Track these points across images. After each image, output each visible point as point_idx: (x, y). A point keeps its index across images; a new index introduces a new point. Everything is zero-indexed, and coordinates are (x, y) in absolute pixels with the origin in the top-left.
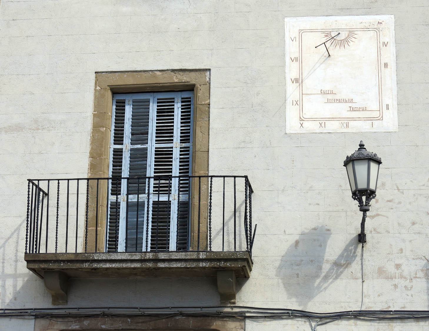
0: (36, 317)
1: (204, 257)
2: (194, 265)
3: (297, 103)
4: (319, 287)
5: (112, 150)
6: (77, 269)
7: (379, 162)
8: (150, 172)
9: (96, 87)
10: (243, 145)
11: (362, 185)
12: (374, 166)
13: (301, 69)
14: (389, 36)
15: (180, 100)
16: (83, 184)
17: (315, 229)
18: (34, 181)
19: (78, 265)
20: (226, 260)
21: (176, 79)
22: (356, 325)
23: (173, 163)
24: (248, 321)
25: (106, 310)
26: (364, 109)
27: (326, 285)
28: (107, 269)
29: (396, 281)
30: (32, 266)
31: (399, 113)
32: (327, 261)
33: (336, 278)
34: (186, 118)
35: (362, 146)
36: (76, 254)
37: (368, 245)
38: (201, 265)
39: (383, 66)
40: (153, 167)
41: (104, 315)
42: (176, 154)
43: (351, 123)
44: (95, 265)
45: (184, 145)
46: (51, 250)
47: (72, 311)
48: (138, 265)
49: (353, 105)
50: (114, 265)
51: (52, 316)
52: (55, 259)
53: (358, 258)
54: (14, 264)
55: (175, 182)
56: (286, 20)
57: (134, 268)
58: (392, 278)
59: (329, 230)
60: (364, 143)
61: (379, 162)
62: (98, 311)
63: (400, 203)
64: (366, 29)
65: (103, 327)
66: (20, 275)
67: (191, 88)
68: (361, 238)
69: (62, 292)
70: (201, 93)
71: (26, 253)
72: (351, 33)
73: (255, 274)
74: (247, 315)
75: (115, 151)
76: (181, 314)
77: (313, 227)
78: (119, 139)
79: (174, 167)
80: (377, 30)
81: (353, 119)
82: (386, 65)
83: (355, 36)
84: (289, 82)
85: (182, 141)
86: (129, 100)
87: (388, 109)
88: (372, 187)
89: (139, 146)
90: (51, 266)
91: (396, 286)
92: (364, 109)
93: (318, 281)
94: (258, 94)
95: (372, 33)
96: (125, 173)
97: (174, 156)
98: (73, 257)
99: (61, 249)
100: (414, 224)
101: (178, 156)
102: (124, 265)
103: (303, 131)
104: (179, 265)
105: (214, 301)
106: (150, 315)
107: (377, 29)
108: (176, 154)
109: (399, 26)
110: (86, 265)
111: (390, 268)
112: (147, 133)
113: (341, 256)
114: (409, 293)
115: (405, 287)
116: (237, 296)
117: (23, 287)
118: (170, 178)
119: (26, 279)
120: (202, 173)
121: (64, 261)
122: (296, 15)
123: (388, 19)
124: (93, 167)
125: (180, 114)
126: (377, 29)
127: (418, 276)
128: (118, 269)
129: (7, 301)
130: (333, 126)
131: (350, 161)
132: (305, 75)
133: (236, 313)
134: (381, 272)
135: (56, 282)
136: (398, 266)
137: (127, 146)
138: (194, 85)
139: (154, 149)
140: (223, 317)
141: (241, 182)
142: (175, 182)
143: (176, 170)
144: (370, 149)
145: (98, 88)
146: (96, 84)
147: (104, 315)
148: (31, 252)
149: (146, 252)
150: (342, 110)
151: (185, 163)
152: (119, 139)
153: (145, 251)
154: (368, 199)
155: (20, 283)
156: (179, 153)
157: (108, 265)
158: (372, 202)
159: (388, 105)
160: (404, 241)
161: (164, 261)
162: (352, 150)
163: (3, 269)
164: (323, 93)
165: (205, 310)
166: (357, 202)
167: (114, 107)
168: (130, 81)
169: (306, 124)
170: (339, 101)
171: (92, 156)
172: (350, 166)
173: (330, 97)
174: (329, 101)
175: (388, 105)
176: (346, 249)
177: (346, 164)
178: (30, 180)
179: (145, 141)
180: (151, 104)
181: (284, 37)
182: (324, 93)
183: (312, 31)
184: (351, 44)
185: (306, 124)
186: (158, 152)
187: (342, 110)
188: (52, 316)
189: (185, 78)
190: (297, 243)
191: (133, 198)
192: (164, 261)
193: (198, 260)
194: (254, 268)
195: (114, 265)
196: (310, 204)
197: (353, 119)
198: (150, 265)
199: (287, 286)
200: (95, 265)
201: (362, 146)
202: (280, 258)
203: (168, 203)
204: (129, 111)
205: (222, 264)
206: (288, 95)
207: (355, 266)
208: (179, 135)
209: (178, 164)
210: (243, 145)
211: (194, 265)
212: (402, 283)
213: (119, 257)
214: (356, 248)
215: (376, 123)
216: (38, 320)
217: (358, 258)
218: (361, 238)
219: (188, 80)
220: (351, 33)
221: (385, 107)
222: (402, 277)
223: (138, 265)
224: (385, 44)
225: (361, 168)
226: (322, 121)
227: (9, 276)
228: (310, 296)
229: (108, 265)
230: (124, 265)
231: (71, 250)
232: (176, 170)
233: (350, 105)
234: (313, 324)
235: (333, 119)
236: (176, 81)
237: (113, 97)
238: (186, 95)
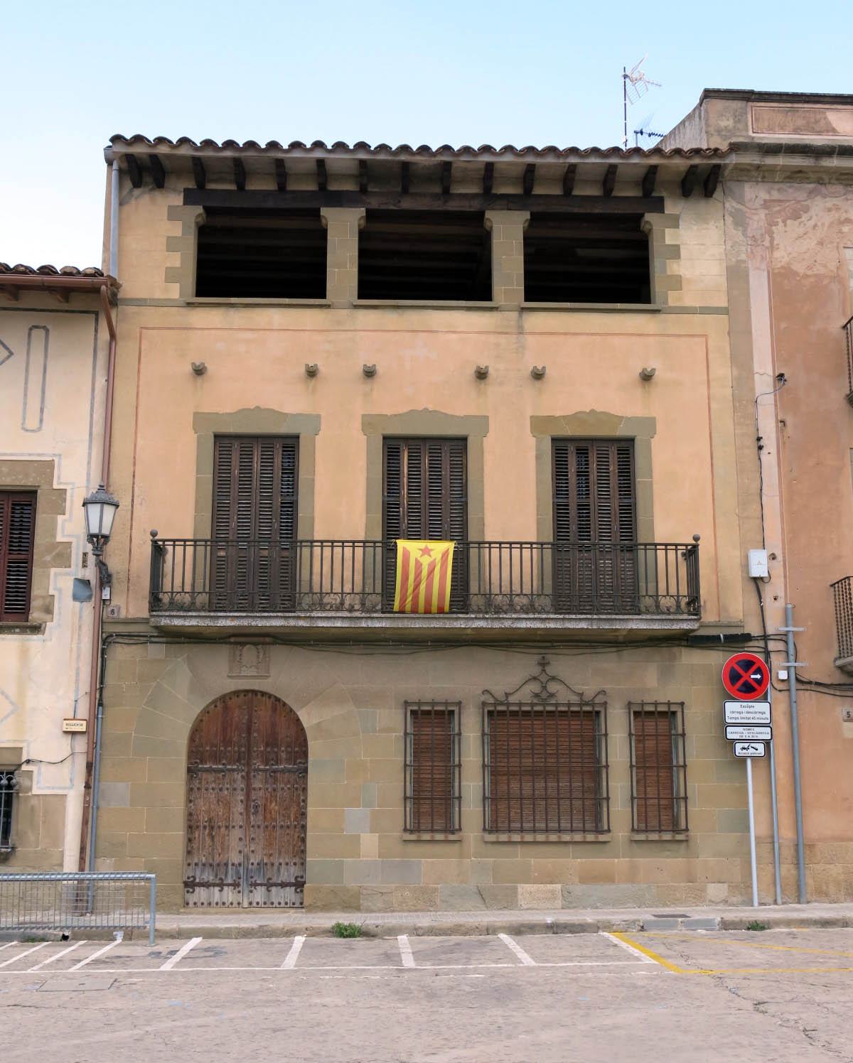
11: (94, 530)
177: (83, 506)
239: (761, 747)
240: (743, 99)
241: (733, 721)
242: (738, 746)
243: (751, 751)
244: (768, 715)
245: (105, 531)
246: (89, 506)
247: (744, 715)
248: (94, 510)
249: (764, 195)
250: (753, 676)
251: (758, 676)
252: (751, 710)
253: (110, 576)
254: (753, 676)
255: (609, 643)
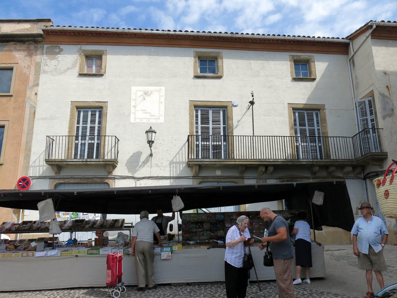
0: (50, 178)
1: (101, 160)
2: (98, 163)
4: (138, 169)
6: (62, 164)
7: (155, 133)
8: (88, 134)
10: (117, 126)
11: (150, 140)
12: (154, 134)
14: (163, 93)
15: (98, 111)
17: (137, 152)
18: (51, 137)
19: (62, 163)
20: (108, 161)
21: (97, 104)
22: (148, 181)
23: (95, 131)
25: (72, 176)
26: (154, 116)
27: (140, 169)
28: (71, 164)
29: (161, 168)
30: (47, 163)
32: (141, 162)
33: (143, 167)
34: (100, 117)
35: (151, 128)
37: (153, 157)
38: (101, 163)
39: (161, 103)
41: (71, 178)
43: (150, 120)
44: (67, 163)
45: (99, 125)
46: (53, 158)
47: (61, 177)
48: (81, 163)
49: (151, 114)
50: (73, 163)
51: (55, 178)
52: (55, 161)
53: (150, 161)
54: (43, 162)
55: (96, 137)
56: (132, 87)
57: (80, 164)
58: (160, 167)
59: (142, 152)
60: (152, 127)
61: (155, 133)
63: (163, 144)
64: (156, 91)
65: (71, 181)
66: (45, 166)
67: (102, 107)
68: (151, 155)
69: (58, 171)
70: (104, 109)
71: (45, 159)
73: (119, 166)
74: (116, 178)
75: (77, 127)
78: (78, 123)
79: (95, 132)
80: (160, 91)
81: (151, 119)
82: (162, 102)
84: (132, 106)
85: (98, 124)
87: (161, 116)
88: (153, 140)
89: (85, 125)
90: (53, 163)
91: (161, 169)
92: (154, 116)
93: (138, 168)
96: (80, 134)
97: (95, 129)
99: (57, 158)
100: (167, 151)
101: (97, 129)
102: (77, 163)
105: (106, 174)
107: (160, 91)
109: (166, 90)
110: (65, 163)
111: (160, 164)
113: (145, 160)
115: (164, 169)
116: (113, 172)
117: (45, 170)
119: (47, 167)
120: (104, 134)
121: (57, 162)
123: (163, 88)
124: (69, 132)
125: (98, 115)
126: (160, 91)
128: (75, 164)
129: (41, 173)
130: (144, 121)
131: (147, 132)
132: (137, 104)
133: (112, 177)
134: (157, 165)
135: (56, 168)
136: (162, 163)
137: (81, 125)
138: (102, 107)
140: (109, 178)
141: (114, 138)
142: (96, 137)
143: (96, 134)
144: (153, 129)
145: (72, 107)
147: (71, 178)
148: (48, 159)
149: (194, 159)
150: (148, 116)
151: (99, 131)
152: (78, 123)
153: (191, 158)
154: (152, 144)
155: (45, 168)
156: (97, 128)
157: (72, 163)
158: (153, 144)
159: (161, 115)
160: (164, 156)
161: (89, 162)
162: (148, 128)
164: (142, 110)
166: (148, 145)
167: (77, 113)
168: (82, 105)
169: (136, 120)
171: (69, 128)
172: (147, 133)
173: (144, 112)
174: (144, 113)
175: (161, 115)
176: (147, 158)
177: (146, 133)
178: (47, 136)
179: (87, 124)
180: (89, 112)
181: (131, 92)
182: (143, 110)
183: (140, 91)
185: (136, 120)
186: (91, 127)
187: (148, 116)
188: (55, 178)
190: (132, 156)
191: (93, 142)
192: (89, 162)
194: (119, 164)
195: (73, 163)
196: (136, 144)
197: (151, 119)
198: (85, 163)
199: (128, 169)
200: (67, 163)
201: (151, 128)
202: (126, 161)
203: (94, 143)
204: (82, 114)
205: (107, 163)
206: (131, 110)
207: (149, 163)
208: (98, 122)
210: (117, 126)
211: (98, 163)
212: (163, 168)
213: (200, 160)
214: (150, 158)
215: (157, 120)
216: (50, 180)
217: (150, 161)
218: (151, 155)
219: (101, 105)
221: (160, 115)
222: (162, 166)
223: (81, 163)
224: (162, 96)
225: (150, 134)
226: (141, 119)
227: (41, 166)
228: (135, 172)
229: (72, 163)
230: (77, 163)
231: (60, 158)
232: (96, 134)
233: (150, 114)
234: (136, 180)
237: (77, 109)
238: (100, 109)
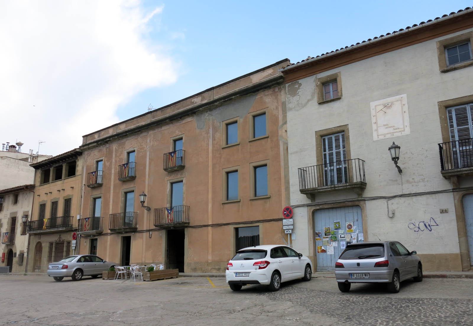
0: (307, 206)
3: (377, 130)
5: (323, 154)
7: (399, 148)
9: (316, 136)
11: (394, 156)
13: (376, 119)
14: (405, 101)
16: (315, 167)
19: (314, 191)
21: (339, 129)
22: (400, 199)
24: (366, 201)
29: (413, 184)
31: (410, 128)
34: (343, 141)
35: (394, 143)
36: (313, 188)
39: (404, 112)
40: (335, 158)
42: (342, 153)
44: (319, 191)
47: (317, 204)
50: (323, 190)
62: (324, 203)
65: (326, 207)
67: (343, 131)
72: (392, 103)
74: (366, 199)
75: (324, 154)
76: (347, 201)
77: (26, 276)
78: (325, 151)
81: (395, 132)
82: (405, 112)
83: (394, 104)
84: (373, 124)
86: (326, 138)
91: (413, 185)
94: (364, 130)
95: (399, 102)
98: (312, 189)
99: (309, 187)
100: (418, 164)
103: (379, 139)
104: (341, 188)
106: (338, 202)
108: (342, 153)
110: (316, 191)
111: (411, 180)
112: (333, 147)
114: (418, 187)
118: (337, 161)
122: (373, 101)
123: (404, 96)
127: (420, 181)
138: (344, 130)
139: (335, 152)
145: (317, 136)
146: (316, 135)
157: (322, 190)
159: (406, 126)
163: (346, 177)
164: (384, 125)
165: (353, 199)
168: (325, 133)
170: (390, 127)
173: (387, 126)
174: (387, 128)
175: (406, 126)
177: (389, 150)
179: (332, 150)
183: (379, 105)
184: (392, 107)
186: (336, 153)
187: (391, 130)
189: (341, 129)
193: (347, 186)
195: (323, 190)
197: (395, 132)
198: (333, 189)
201: (394, 143)
209: (343, 155)
215: (402, 132)
220: (392, 103)
221: (405, 127)
222: (415, 182)
223: (330, 189)
224: (404, 105)
226: (384, 135)
229: (322, 190)
231: (312, 187)
235: (387, 134)
236: (339, 130)
238: (343, 133)
239: (291, 231)
240: (207, 91)
241: (285, 224)
242: (286, 231)
243: (289, 232)
244: (292, 222)
245: (397, 156)
246: (391, 149)
247: (287, 223)
248: (393, 151)
249: (87, 153)
250: (286, 213)
251: (285, 213)
252: (289, 221)
253: (401, 170)
254: (286, 213)
255: (385, 198)
